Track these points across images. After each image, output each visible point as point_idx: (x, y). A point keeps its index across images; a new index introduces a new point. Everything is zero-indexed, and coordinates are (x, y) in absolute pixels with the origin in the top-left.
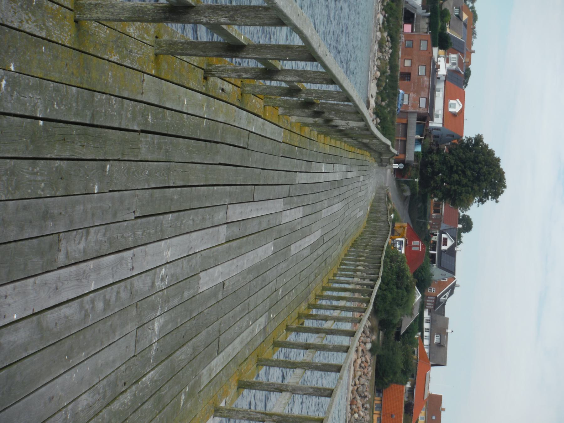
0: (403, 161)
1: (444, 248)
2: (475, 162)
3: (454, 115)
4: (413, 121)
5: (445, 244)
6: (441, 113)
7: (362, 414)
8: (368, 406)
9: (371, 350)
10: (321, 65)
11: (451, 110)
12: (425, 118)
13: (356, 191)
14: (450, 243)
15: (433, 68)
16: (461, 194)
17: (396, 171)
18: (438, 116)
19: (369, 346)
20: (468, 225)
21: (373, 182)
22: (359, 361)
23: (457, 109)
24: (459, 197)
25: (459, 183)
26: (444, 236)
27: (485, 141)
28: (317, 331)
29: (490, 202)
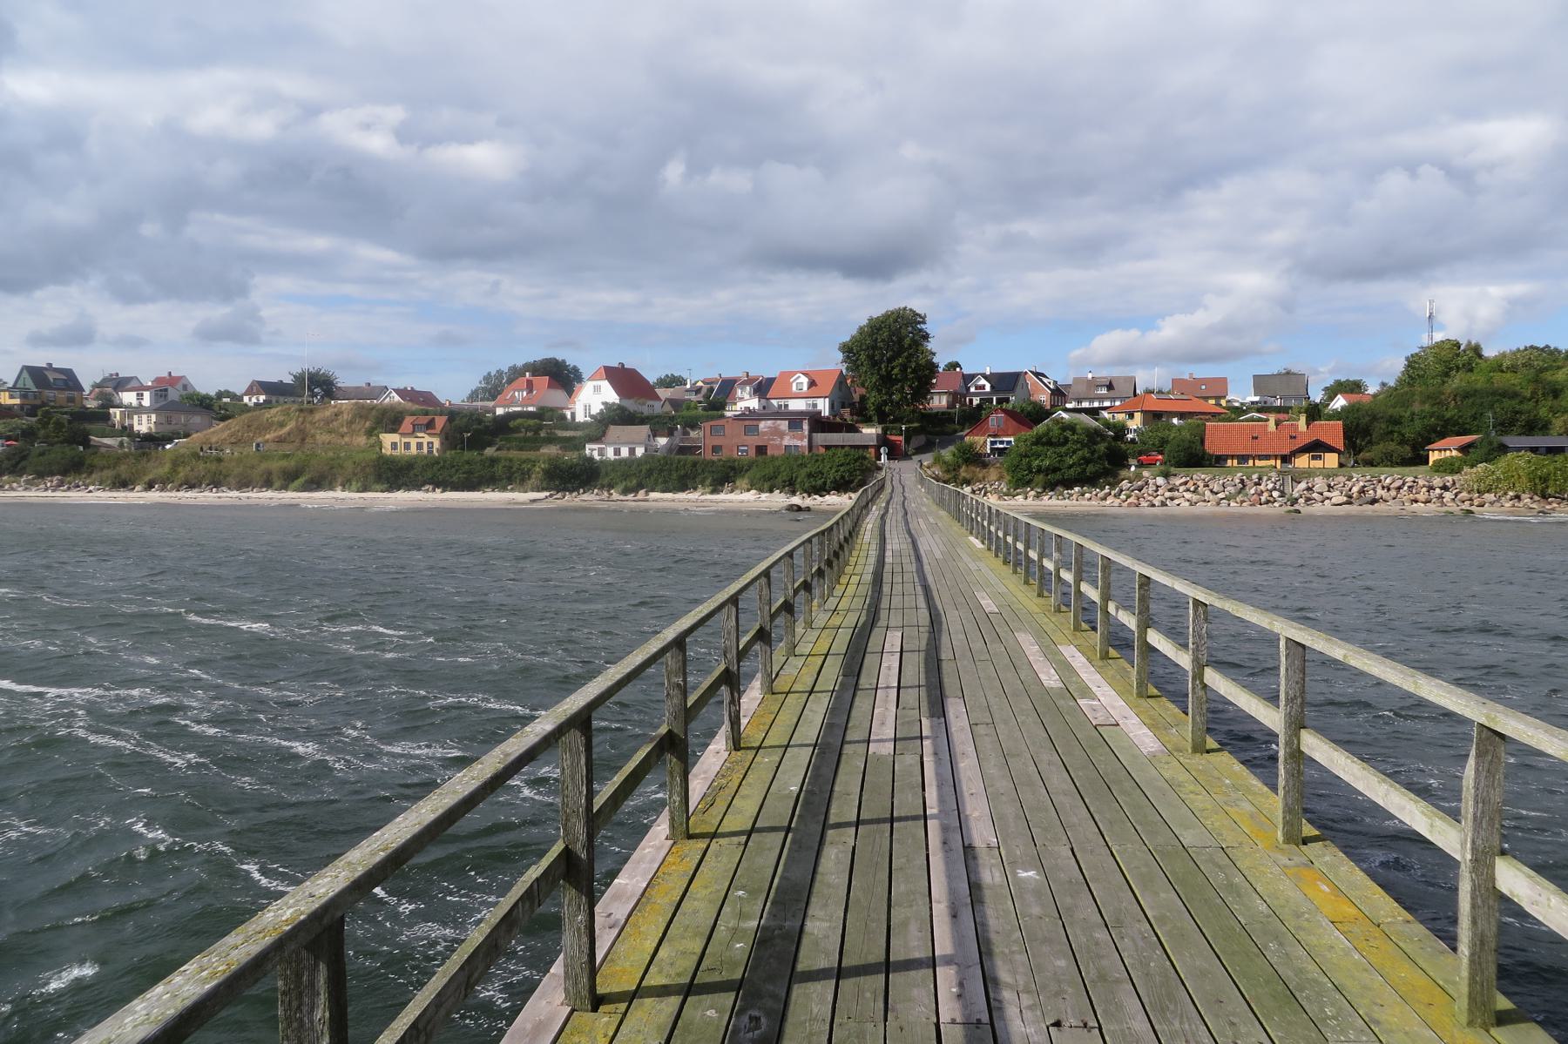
0: (877, 448)
1: (988, 388)
2: (874, 348)
3: (812, 384)
4: (820, 438)
5: (983, 387)
6: (810, 401)
7: (1271, 486)
8: (1255, 477)
9: (1166, 475)
10: (468, 811)
11: (805, 388)
12: (819, 424)
13: (919, 515)
14: (983, 382)
15: (749, 415)
16: (918, 364)
17: (891, 456)
18: (815, 405)
19: (1160, 481)
20: (954, 366)
21: (910, 480)
22: (1188, 495)
23: (804, 380)
24: (925, 375)
25: (904, 368)
26: (972, 390)
27: (847, 339)
28: (1521, 818)
29: (928, 327)
